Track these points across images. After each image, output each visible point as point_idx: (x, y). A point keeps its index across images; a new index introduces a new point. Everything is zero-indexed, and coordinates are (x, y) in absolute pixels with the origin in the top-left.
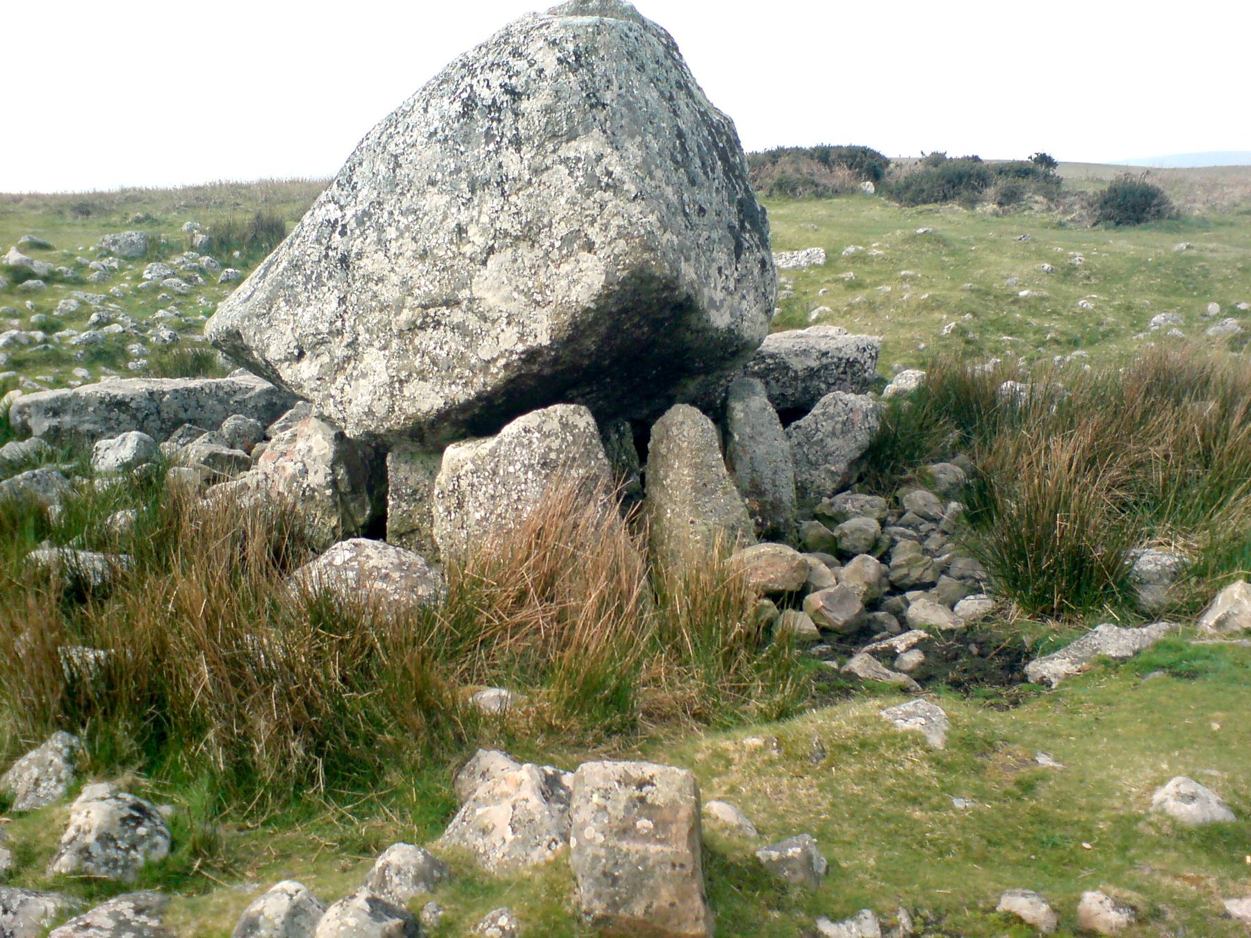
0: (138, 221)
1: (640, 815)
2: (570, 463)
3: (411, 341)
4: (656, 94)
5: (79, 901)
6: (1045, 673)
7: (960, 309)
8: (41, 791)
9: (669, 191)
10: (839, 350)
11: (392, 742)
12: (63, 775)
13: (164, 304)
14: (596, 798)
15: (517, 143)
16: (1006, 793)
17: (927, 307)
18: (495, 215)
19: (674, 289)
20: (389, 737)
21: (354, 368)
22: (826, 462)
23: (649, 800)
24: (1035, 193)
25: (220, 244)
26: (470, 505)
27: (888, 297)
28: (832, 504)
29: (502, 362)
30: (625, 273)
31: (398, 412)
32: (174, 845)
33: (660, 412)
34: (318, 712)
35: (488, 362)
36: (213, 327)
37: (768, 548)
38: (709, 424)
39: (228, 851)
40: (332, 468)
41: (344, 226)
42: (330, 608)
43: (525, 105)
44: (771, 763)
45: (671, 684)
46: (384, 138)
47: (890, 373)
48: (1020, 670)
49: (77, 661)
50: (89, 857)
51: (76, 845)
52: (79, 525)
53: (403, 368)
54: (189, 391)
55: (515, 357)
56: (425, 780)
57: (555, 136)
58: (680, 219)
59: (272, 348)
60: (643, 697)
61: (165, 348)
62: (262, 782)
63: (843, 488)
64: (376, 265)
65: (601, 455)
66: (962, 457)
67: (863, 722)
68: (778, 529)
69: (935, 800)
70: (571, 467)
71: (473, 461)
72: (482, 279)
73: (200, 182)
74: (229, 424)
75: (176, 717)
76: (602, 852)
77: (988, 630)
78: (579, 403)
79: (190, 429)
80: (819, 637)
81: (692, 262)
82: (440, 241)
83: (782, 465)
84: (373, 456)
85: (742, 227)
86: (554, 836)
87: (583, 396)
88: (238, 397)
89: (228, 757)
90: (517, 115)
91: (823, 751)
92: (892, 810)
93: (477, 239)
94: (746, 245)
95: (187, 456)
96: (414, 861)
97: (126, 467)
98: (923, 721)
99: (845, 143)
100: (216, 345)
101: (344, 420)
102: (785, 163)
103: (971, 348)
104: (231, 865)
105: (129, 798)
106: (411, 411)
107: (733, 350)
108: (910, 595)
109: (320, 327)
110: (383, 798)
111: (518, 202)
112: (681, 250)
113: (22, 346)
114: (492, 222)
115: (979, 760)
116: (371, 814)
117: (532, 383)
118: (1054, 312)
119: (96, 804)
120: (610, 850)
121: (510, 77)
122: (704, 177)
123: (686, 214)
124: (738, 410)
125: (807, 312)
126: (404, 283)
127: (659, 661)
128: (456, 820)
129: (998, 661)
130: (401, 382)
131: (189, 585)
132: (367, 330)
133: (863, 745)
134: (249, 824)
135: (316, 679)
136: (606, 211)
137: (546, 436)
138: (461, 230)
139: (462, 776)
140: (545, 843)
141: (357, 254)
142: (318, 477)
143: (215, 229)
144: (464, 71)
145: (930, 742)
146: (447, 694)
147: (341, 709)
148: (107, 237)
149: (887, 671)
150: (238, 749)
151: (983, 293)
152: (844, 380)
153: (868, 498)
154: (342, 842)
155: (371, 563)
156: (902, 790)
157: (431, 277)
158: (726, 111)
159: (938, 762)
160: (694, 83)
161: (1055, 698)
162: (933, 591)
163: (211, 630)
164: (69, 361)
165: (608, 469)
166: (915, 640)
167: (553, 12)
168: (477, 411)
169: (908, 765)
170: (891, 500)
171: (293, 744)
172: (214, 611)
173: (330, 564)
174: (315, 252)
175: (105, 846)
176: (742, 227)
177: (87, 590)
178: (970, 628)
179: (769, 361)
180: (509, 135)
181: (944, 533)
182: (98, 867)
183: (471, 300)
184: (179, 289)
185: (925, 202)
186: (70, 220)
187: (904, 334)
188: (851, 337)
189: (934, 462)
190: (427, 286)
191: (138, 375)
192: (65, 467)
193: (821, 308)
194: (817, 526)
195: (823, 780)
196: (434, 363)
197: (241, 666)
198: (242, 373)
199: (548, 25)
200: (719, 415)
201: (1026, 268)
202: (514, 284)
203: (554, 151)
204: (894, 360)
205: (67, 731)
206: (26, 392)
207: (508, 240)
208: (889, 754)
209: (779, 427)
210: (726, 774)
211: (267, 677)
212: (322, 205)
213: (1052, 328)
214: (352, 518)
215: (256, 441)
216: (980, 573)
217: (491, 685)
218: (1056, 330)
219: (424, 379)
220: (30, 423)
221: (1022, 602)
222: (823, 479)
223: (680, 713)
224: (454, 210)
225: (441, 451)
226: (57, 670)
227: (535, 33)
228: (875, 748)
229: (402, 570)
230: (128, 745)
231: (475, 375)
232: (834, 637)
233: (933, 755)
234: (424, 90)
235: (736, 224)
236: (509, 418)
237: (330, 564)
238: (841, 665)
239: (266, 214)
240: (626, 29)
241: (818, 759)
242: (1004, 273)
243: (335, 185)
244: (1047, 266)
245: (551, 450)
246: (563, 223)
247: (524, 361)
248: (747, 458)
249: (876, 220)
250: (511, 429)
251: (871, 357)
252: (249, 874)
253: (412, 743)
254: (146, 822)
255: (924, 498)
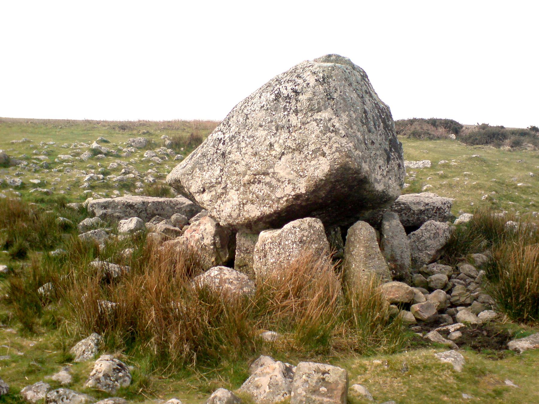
0: (144, 133)
1: (322, 386)
2: (312, 242)
3: (249, 188)
4: (356, 95)
5: (94, 398)
6: (517, 346)
7: (490, 189)
8: (85, 355)
9: (359, 134)
10: (434, 203)
11: (226, 349)
12: (94, 350)
13: (151, 167)
14: (304, 377)
15: (296, 112)
16: (488, 394)
17: (475, 188)
18: (285, 140)
19: (359, 174)
20: (224, 347)
21: (225, 198)
22: (426, 250)
23: (326, 380)
24: (528, 143)
25: (176, 145)
26: (269, 256)
27: (458, 182)
28: (427, 268)
29: (285, 199)
30: (338, 166)
31: (241, 217)
32: (132, 382)
33: (352, 224)
34: (197, 335)
35: (280, 198)
36: (170, 177)
37: (396, 283)
38: (373, 230)
39: (154, 386)
40: (214, 237)
41: (224, 141)
42: (207, 293)
43: (300, 97)
44: (384, 371)
45: (347, 336)
46: (243, 107)
47: (458, 214)
48: (506, 344)
49: (104, 306)
50: (99, 383)
51: (95, 377)
52: (111, 253)
53: (245, 199)
54: (159, 202)
55: (291, 197)
56: (237, 366)
57: (312, 110)
58: (363, 146)
59: (193, 188)
60: (333, 342)
61: (151, 184)
62: (171, 360)
63: (433, 261)
64: (236, 157)
65: (325, 240)
66: (488, 252)
67: (426, 358)
68: (402, 276)
69: (454, 393)
70: (312, 243)
71: (271, 239)
72: (278, 165)
73: (170, 119)
74: (174, 217)
75: (140, 331)
76: (304, 399)
77: (492, 326)
78: (317, 218)
79: (158, 218)
80: (416, 323)
81: (367, 163)
82: (262, 149)
83: (405, 250)
84: (230, 234)
85: (391, 150)
86: (286, 391)
87: (319, 215)
88: (179, 206)
89: (158, 349)
90: (297, 101)
91: (407, 368)
92: (434, 395)
93: (278, 149)
94: (392, 157)
95: (156, 229)
96: (227, 396)
97: (131, 231)
98: (453, 360)
99: (443, 118)
100: (170, 185)
101: (220, 218)
102: (416, 125)
103: (494, 206)
104: (154, 392)
105: (117, 361)
106: (247, 216)
107: (384, 200)
108: (458, 308)
109: (212, 180)
110: (220, 372)
111: (295, 135)
112: (363, 158)
113: (95, 180)
114: (284, 142)
115: (477, 378)
116: (213, 377)
117: (297, 208)
118: (534, 193)
119: (104, 362)
120: (307, 398)
121: (295, 86)
122: (374, 130)
123: (366, 144)
124: (386, 225)
125: (422, 186)
126: (247, 165)
127: (343, 327)
128: (246, 382)
129: (495, 339)
130: (243, 204)
131: (151, 279)
132: (231, 183)
133: (425, 367)
134: (163, 377)
135: (198, 320)
136: (331, 141)
137: (302, 230)
138: (271, 145)
139: (253, 366)
140: (282, 394)
141: (229, 152)
142: (208, 240)
143: (174, 139)
144: (277, 82)
145: (455, 368)
146: (250, 332)
147: (206, 333)
148: (131, 139)
149: (444, 339)
150: (163, 346)
151: (501, 183)
152: (436, 216)
153: (444, 266)
154: (200, 387)
155: (226, 276)
156: (440, 387)
157: (258, 163)
158: (386, 103)
159: (458, 377)
160: (374, 91)
161: (520, 358)
162: (469, 307)
163: (158, 298)
164: (113, 187)
165: (328, 246)
166: (459, 327)
167: (315, 61)
168: (274, 218)
169: (444, 377)
170: (454, 268)
171: (185, 346)
172: (160, 290)
173: (209, 276)
174: (212, 150)
175: (106, 379)
176: (391, 150)
177: (111, 278)
178: (484, 324)
179: (402, 206)
180: (293, 108)
181: (477, 283)
182: (102, 386)
183: (274, 173)
184: (158, 162)
185: (477, 144)
186: (117, 132)
187: (465, 198)
188: (439, 198)
189: (475, 253)
190: (256, 167)
191: (139, 195)
192: (107, 230)
193: (428, 185)
194: (420, 276)
195: (405, 380)
196: (257, 197)
197: (168, 313)
198: (181, 197)
199: (312, 66)
200: (378, 226)
201: (521, 174)
202: (292, 167)
203: (311, 116)
204: (460, 209)
205: (97, 333)
206: (94, 198)
207: (290, 150)
208: (436, 372)
209: (405, 234)
210: (364, 374)
211: (177, 318)
212: (216, 132)
213: (533, 200)
214: (221, 258)
215: (185, 225)
216: (491, 301)
217: (270, 330)
218: (534, 201)
219: (253, 204)
220: (95, 211)
221: (509, 315)
222: (424, 257)
223: (349, 348)
224: (269, 137)
225: (258, 233)
226: (96, 309)
227: (307, 69)
228: (430, 369)
229: (238, 280)
230: (119, 341)
231: (274, 203)
232: (423, 323)
233: (456, 374)
234: (260, 89)
235: (388, 149)
236: (287, 222)
237: (209, 276)
238: (424, 335)
239: (195, 134)
240: (345, 69)
241: (404, 371)
242: (511, 176)
243: (222, 124)
244: (531, 174)
245: (304, 236)
246: (313, 145)
247: (294, 199)
248: (389, 246)
249: (455, 150)
250: (288, 226)
251: (448, 207)
252: (160, 396)
253: (234, 350)
254: (123, 371)
255: (469, 268)
